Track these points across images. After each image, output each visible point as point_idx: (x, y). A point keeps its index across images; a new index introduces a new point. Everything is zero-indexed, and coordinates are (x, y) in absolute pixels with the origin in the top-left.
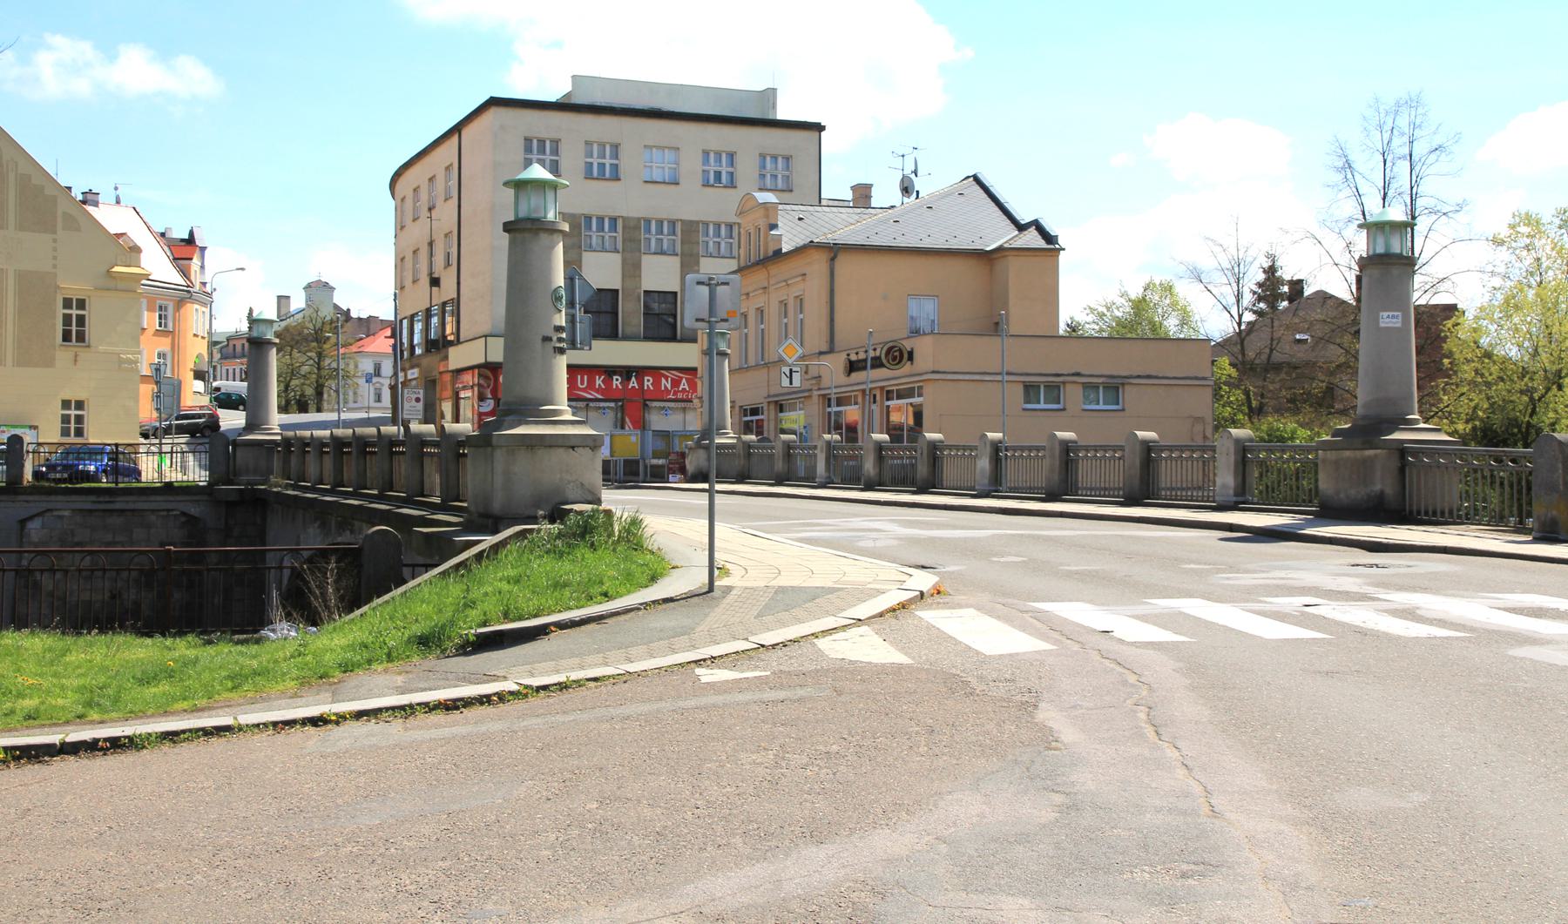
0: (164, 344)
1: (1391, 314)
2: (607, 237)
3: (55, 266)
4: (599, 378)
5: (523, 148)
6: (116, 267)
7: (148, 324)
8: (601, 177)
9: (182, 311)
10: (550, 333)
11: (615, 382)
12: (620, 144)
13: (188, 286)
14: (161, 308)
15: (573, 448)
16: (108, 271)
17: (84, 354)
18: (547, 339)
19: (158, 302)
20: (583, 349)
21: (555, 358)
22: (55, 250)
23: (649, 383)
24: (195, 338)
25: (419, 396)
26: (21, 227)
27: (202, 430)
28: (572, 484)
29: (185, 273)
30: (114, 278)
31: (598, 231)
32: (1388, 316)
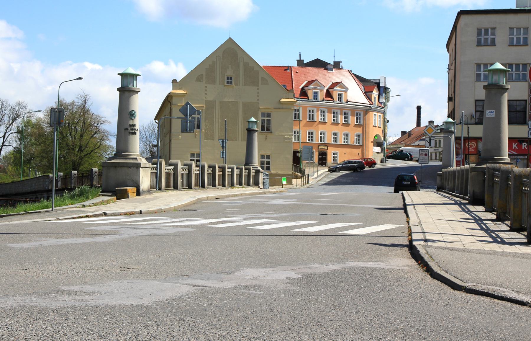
0: (359, 131)
1: (490, 111)
2: (521, 74)
3: (258, 100)
4: (515, 144)
5: (476, 34)
6: (283, 99)
7: (351, 122)
8: (518, 44)
9: (367, 116)
10: (128, 127)
11: (523, 146)
12: (528, 27)
13: (370, 104)
14: (357, 114)
15: (130, 167)
16: (280, 101)
17: (269, 136)
18: (126, 129)
19: (356, 112)
20: (191, 132)
21: (129, 136)
22: (258, 93)
23: (525, 146)
24: (375, 128)
25: (426, 153)
26: (245, 84)
27: (356, 168)
28: (129, 180)
29: (369, 98)
30: (282, 103)
31: (516, 71)
32: (489, 113)
